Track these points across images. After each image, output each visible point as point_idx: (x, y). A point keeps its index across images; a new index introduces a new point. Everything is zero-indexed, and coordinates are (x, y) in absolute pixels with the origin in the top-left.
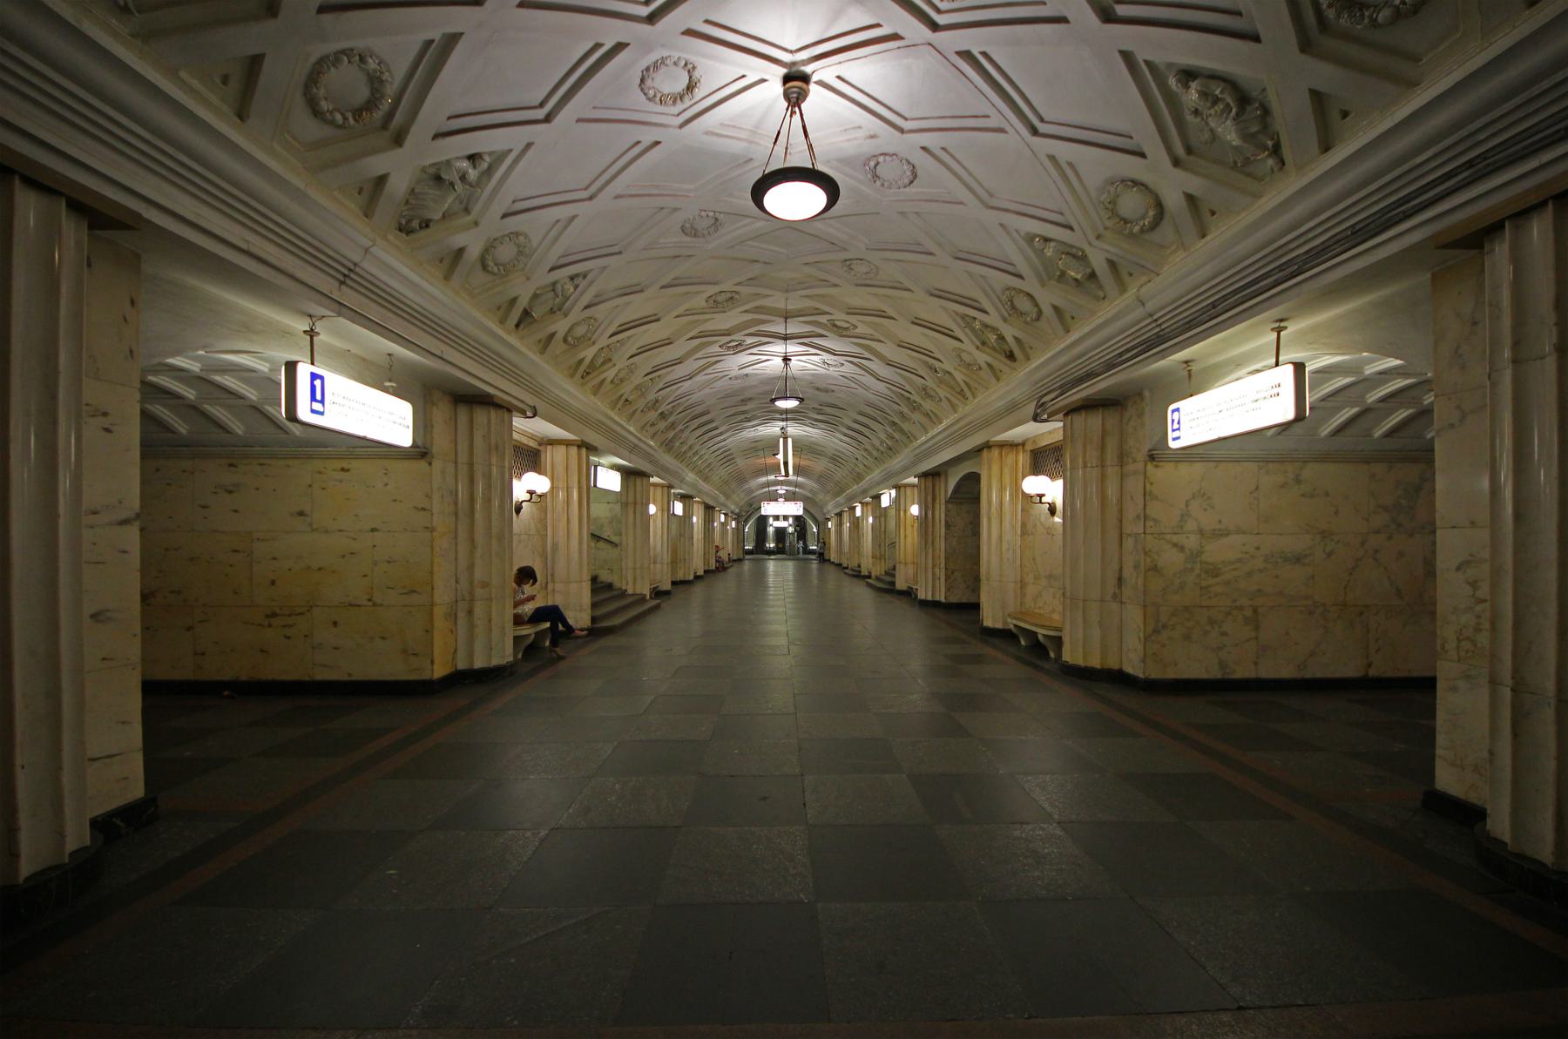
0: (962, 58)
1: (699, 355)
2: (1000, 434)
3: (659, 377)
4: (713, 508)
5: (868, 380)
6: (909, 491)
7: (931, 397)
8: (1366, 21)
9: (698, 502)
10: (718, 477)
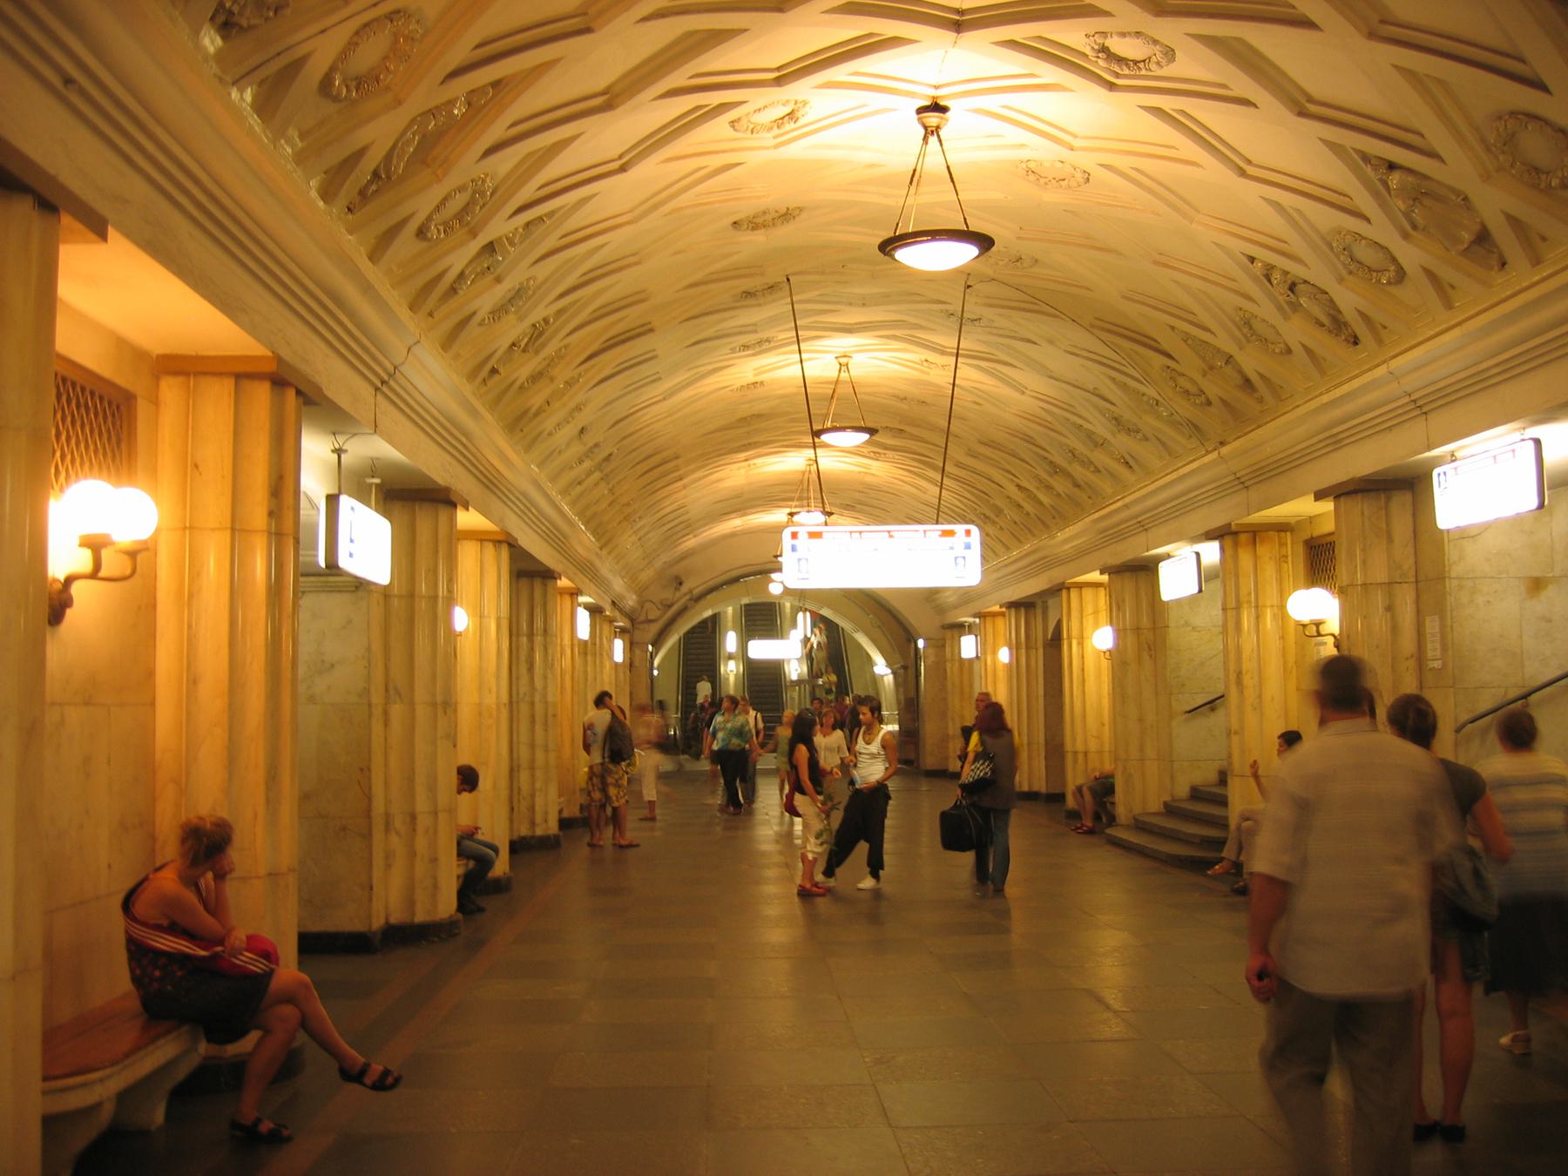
0: (1149, 112)
1: (678, 78)
2: (1425, 452)
3: (496, 84)
4: (548, 575)
5: (1005, 391)
6: (1088, 593)
7: (1096, 445)
8: (1374, 280)
9: (479, 537)
10: (570, 430)
